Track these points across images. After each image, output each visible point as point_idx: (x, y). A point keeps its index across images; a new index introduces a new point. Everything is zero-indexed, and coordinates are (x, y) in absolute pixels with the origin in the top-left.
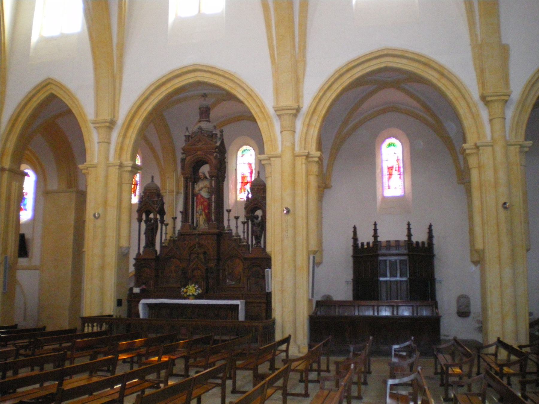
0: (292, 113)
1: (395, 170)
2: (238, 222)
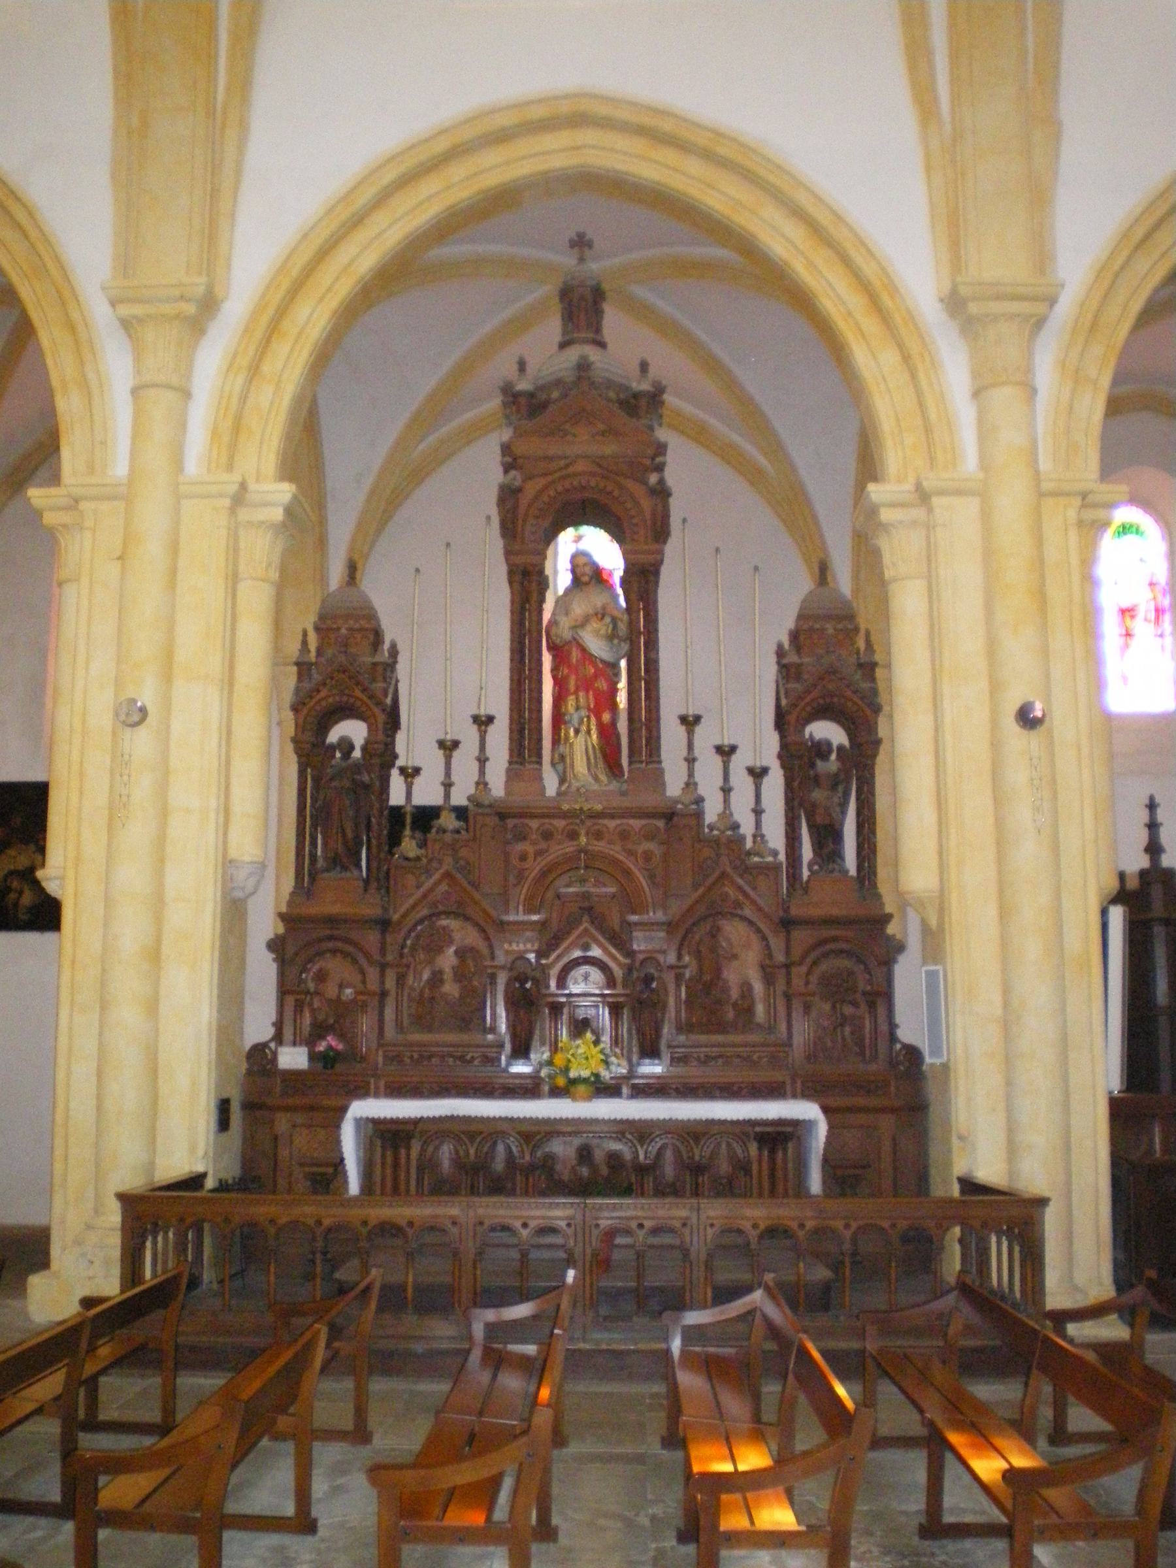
0: (1031, 316)
1: (1146, 620)
2: (732, 766)
